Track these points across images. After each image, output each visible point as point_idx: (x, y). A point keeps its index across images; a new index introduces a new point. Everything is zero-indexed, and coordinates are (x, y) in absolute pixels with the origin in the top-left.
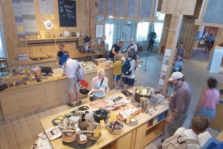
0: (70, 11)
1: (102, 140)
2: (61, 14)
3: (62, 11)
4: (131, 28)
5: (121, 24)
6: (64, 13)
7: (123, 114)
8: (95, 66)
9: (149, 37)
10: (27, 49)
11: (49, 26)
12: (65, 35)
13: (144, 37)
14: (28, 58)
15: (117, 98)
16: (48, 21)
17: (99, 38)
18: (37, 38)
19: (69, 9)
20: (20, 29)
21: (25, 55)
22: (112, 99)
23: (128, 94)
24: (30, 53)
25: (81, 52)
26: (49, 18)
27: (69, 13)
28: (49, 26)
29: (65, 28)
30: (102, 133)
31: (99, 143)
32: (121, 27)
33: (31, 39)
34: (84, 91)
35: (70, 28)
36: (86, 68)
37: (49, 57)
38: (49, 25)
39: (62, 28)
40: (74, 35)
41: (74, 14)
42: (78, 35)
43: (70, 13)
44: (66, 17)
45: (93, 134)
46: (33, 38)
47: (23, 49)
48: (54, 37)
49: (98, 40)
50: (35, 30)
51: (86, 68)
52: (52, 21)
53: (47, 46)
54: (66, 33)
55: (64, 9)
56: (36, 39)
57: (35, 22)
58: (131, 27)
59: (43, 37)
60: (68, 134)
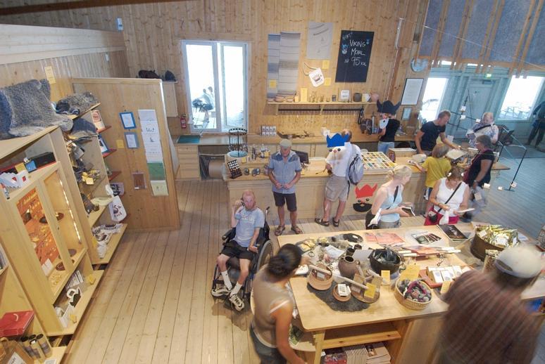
0: (359, 52)
1: (380, 307)
2: (341, 57)
3: (344, 52)
4: (492, 88)
5: (468, 77)
6: (349, 56)
7: (434, 273)
8: (389, 161)
9: (538, 113)
10: (276, 118)
11: (316, 81)
12: (342, 98)
13: (521, 112)
14: (275, 133)
15: (427, 236)
16: (318, 72)
17: (408, 106)
18: (294, 101)
19: (359, 48)
20: (273, 85)
21: (271, 128)
22: (415, 236)
23: (455, 233)
24: (280, 125)
25: (366, 131)
26: (320, 65)
27: (357, 56)
28: (316, 81)
29: (343, 84)
30: (381, 295)
31: (372, 311)
32: (466, 84)
33: (285, 103)
34: (362, 205)
35: (354, 85)
36: (369, 164)
37: (307, 136)
38: (317, 78)
39: (338, 84)
40: (357, 97)
41: (366, 59)
42: (366, 97)
43: (359, 55)
44: (351, 63)
45: (363, 290)
46: (289, 100)
47: (271, 117)
48: (322, 101)
49: (406, 110)
50: (292, 88)
51: (369, 164)
52: (324, 71)
53: (307, 116)
54: (345, 93)
55: (349, 49)
56: (293, 103)
57: (295, 72)
58: (490, 86)
59: (303, 99)
60: (319, 275)
